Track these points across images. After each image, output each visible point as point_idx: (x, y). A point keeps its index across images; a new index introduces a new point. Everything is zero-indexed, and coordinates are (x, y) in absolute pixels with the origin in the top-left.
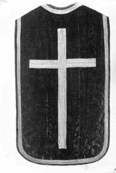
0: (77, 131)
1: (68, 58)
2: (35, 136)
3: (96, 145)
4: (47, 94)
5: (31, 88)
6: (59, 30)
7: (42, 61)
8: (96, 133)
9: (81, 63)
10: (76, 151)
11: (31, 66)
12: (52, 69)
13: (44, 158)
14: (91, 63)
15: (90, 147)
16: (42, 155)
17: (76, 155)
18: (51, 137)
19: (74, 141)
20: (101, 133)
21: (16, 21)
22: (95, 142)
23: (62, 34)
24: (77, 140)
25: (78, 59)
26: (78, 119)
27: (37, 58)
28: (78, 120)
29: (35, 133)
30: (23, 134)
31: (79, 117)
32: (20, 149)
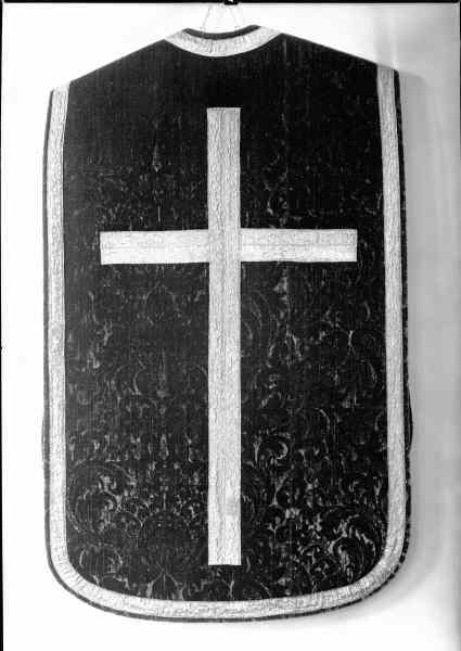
0: (277, 489)
2: (119, 506)
3: (354, 534)
5: (101, 327)
6: (213, 115)
11: (107, 258)
14: (336, 247)
15: (331, 546)
16: (148, 581)
17: (283, 581)
18: (178, 514)
20: (373, 492)
22: (349, 526)
23: (223, 128)
24: (281, 522)
26: (284, 446)
27: (124, 224)
28: (282, 448)
29: (118, 498)
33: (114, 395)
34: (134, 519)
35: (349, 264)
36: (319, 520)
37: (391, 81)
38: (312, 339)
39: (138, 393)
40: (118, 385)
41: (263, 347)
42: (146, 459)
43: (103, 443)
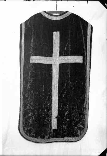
1: (61, 56)
4: (43, 85)
6: (54, 33)
7: (40, 57)
8: (81, 117)
9: (70, 59)
10: (65, 130)
12: (48, 65)
13: (40, 137)
14: (78, 59)
15: (76, 128)
19: (64, 123)
21: (21, 25)
23: (56, 36)
24: (66, 122)
25: (68, 56)
30: (24, 118)
31: (68, 103)
32: (21, 130)
33: (33, 94)
34: (37, 122)
35: (60, 32)
36: (74, 122)
37: (91, 28)
38: (74, 83)
39: (38, 94)
40: (33, 92)
41: (64, 84)
42: (39, 108)
43: (30, 105)
